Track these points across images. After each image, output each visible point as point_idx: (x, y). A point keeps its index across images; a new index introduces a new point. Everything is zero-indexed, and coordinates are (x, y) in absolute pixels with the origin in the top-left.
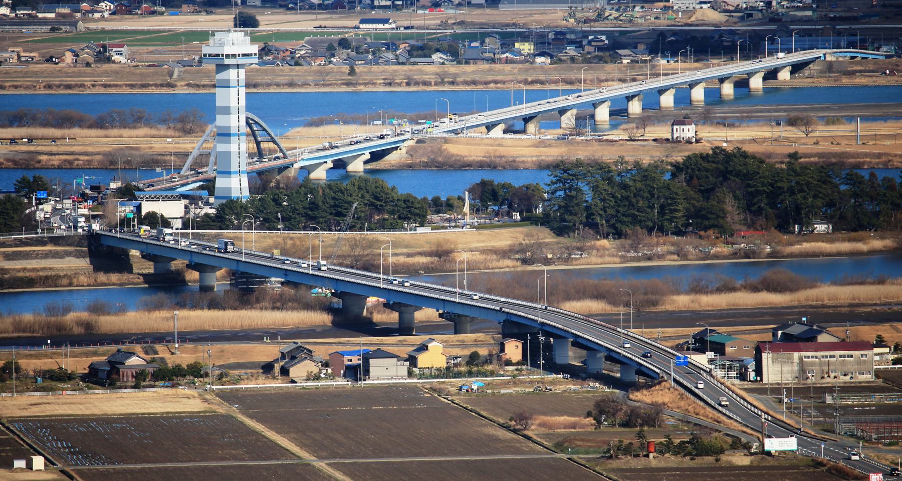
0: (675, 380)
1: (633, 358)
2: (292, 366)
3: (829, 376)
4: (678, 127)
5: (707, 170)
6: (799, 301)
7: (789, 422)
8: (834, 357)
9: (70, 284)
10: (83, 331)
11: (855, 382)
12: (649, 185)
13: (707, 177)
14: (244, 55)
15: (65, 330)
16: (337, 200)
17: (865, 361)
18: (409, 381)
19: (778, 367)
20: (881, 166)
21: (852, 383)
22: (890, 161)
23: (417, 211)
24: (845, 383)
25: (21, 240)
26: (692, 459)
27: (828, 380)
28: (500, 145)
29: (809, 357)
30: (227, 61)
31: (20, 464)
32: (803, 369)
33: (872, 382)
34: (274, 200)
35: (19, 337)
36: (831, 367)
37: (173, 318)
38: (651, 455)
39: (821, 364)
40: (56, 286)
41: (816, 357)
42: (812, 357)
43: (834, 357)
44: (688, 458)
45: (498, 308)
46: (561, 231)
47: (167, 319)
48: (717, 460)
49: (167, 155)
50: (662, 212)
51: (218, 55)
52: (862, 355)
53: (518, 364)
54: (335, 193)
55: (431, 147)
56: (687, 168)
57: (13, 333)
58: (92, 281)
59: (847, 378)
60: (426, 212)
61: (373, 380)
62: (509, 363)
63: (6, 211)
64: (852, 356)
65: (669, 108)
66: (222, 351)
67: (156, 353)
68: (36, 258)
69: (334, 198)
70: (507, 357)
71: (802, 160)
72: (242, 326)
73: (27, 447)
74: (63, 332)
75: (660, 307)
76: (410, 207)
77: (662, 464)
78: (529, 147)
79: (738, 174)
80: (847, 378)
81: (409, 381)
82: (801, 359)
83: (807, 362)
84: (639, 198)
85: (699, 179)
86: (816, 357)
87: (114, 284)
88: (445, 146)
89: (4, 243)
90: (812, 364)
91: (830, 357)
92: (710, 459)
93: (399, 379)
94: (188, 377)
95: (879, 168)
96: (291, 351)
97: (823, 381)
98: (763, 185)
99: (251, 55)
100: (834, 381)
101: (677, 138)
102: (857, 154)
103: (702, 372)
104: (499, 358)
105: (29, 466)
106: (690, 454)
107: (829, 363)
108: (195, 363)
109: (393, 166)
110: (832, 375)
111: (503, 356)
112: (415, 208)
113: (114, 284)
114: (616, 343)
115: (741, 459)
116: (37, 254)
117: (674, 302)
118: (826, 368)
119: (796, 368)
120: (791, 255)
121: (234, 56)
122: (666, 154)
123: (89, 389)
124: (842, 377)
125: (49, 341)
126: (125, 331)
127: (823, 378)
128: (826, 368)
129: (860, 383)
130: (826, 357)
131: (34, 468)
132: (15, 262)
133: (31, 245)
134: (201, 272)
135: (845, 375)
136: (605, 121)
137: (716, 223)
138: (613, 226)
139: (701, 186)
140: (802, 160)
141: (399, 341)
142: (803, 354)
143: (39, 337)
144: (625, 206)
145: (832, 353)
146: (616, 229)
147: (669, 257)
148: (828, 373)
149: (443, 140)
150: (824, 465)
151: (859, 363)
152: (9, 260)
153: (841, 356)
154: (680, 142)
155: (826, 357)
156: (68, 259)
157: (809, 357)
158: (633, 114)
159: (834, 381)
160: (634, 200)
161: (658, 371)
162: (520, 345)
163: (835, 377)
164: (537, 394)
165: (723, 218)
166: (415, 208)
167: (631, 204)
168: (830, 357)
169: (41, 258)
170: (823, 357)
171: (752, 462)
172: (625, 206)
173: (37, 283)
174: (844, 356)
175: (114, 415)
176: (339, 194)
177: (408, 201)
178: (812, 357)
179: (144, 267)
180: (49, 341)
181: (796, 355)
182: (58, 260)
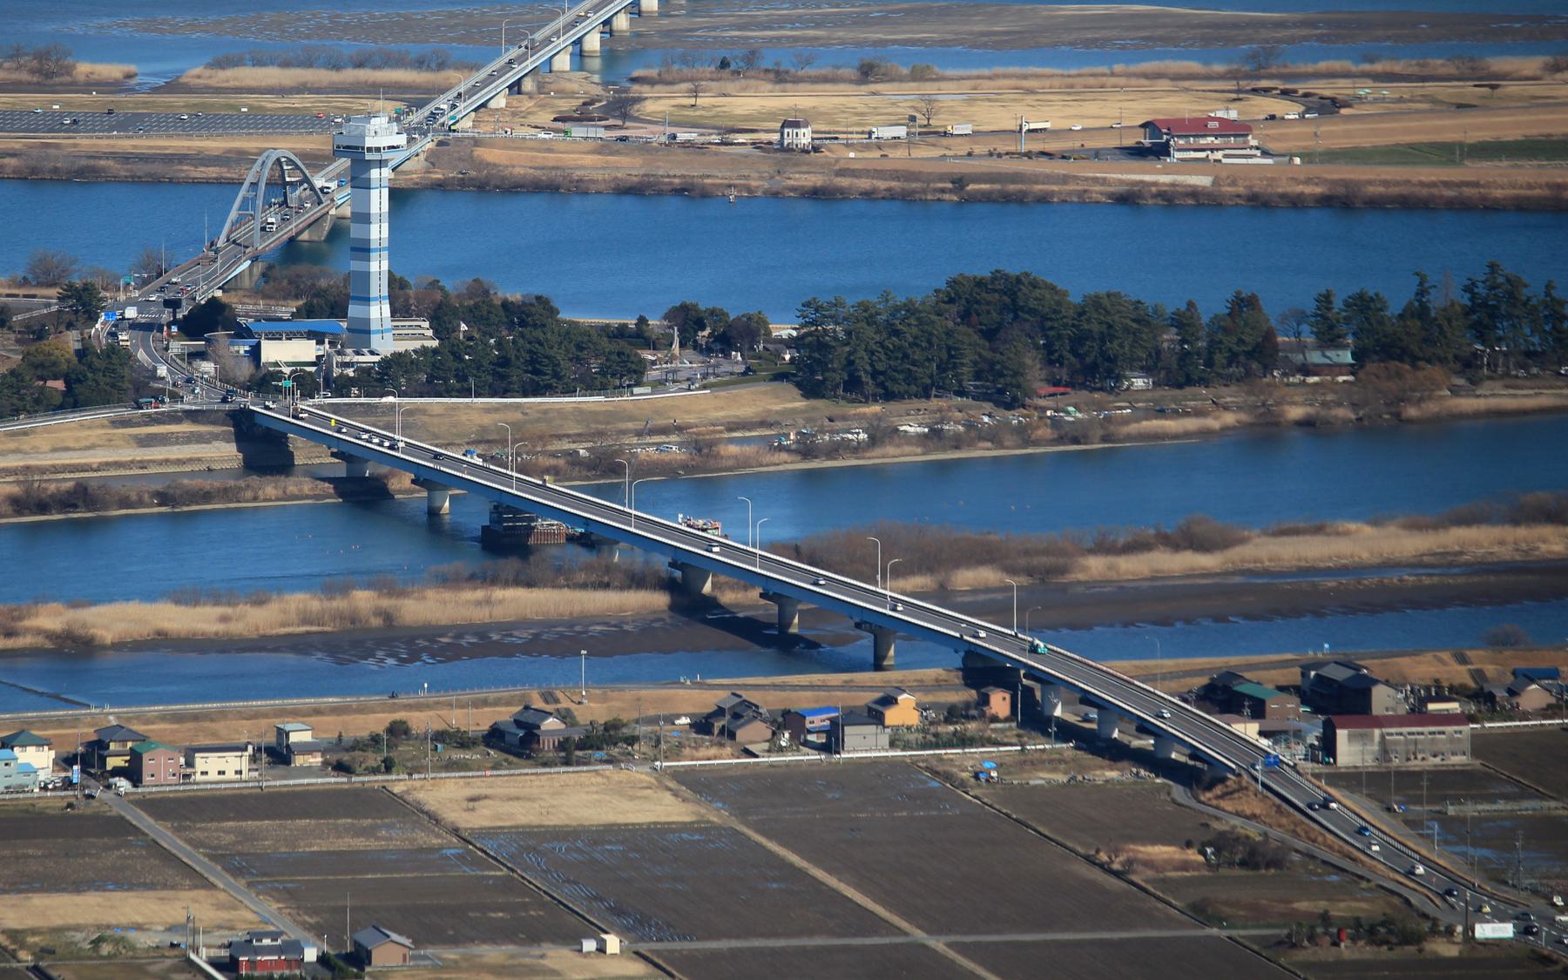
0: (1264, 785)
1: (1187, 739)
2: (739, 727)
3: (1416, 758)
4: (790, 130)
5: (989, 303)
6: (1233, 563)
7: (1441, 862)
8: (1422, 734)
9: (255, 499)
10: (381, 622)
11: (1447, 765)
12: (927, 332)
13: (988, 312)
14: (389, 147)
15: (361, 621)
16: (535, 353)
17: (1459, 739)
18: (891, 754)
19: (1357, 748)
20: (1075, 199)
21: (1443, 765)
22: (1085, 191)
23: (634, 367)
24: (1435, 766)
25: (149, 415)
26: (1390, 949)
27: (1416, 762)
28: (550, 150)
29: (1392, 734)
30: (368, 156)
31: (589, 945)
32: (1385, 750)
33: (1468, 765)
34: (453, 353)
35: (308, 633)
36: (1420, 747)
37: (488, 602)
38: (1343, 945)
39: (1407, 742)
40: (239, 502)
41: (1401, 734)
42: (1397, 734)
43: (1422, 734)
44: (1385, 947)
45: (958, 635)
46: (811, 390)
47: (478, 603)
48: (1420, 951)
49: (100, 158)
50: (942, 368)
51: (357, 148)
52: (1456, 732)
53: (1006, 720)
54: (530, 343)
55: (459, 152)
56: (960, 298)
57: (298, 625)
58: (280, 493)
59: (1437, 760)
60: (645, 368)
61: (849, 752)
62: (995, 719)
63: (112, 367)
64: (1443, 733)
65: (652, 12)
66: (639, 699)
67: (557, 701)
68: (177, 443)
69: (530, 351)
70: (993, 711)
71: (971, 187)
72: (571, 614)
73: (549, 899)
74: (358, 625)
75: (1073, 576)
76: (625, 362)
77: (1356, 956)
78: (588, 153)
79: (1032, 311)
80: (1437, 760)
81: (891, 754)
82: (1382, 737)
83: (1390, 741)
84: (915, 349)
85: (978, 315)
86: (1401, 734)
87: (307, 497)
88: (480, 152)
89: (130, 420)
90: (1396, 743)
91: (1419, 734)
92: (1411, 949)
93: (879, 750)
94: (620, 744)
95: (1072, 202)
96: (733, 706)
97: (1410, 763)
98: (1065, 326)
99: (398, 147)
100: (1422, 763)
101: (788, 144)
102: (1036, 175)
103: (1285, 767)
104: (983, 714)
105: (601, 950)
106: (1387, 942)
107: (1416, 742)
108: (614, 720)
109: (417, 184)
110: (1420, 756)
111: (987, 712)
112: (632, 363)
113: (307, 497)
114: (1147, 708)
115: (1446, 949)
116: (177, 438)
117: (1085, 569)
118: (1412, 748)
119: (1376, 748)
120: (1129, 438)
121: (378, 150)
122: (776, 168)
123: (510, 765)
124: (1432, 758)
125: (426, 685)
126: (433, 623)
127: (1408, 759)
128: (1412, 748)
129: (1453, 765)
130: (1413, 734)
131: (608, 952)
132: (152, 449)
133: (164, 423)
134: (429, 490)
135: (1435, 756)
136: (595, 52)
137: (1014, 382)
138: (882, 385)
139: (981, 324)
140: (971, 187)
141: (845, 682)
142: (1385, 730)
143: (331, 633)
144: (897, 358)
145: (1420, 729)
146: (885, 388)
147: (981, 444)
148: (1415, 754)
149: (472, 142)
150: (1556, 962)
151: (1452, 740)
152: (144, 446)
153: (1430, 733)
154: (793, 150)
155: (1413, 734)
156: (216, 444)
157: (1392, 734)
158: (618, 31)
159: (1422, 763)
160: (909, 351)
161: (1233, 766)
162: (1008, 696)
163: (1423, 759)
164: (1074, 786)
165: (1022, 375)
166: (632, 363)
167: (906, 356)
168: (1419, 734)
169: (183, 443)
170: (1409, 734)
171: (1460, 952)
172: (897, 358)
173: (215, 497)
174: (1434, 733)
175: (592, 826)
176: (537, 346)
177: (623, 354)
178: (1397, 734)
179: (314, 455)
180: (426, 685)
181: (1377, 732)
182: (204, 445)
